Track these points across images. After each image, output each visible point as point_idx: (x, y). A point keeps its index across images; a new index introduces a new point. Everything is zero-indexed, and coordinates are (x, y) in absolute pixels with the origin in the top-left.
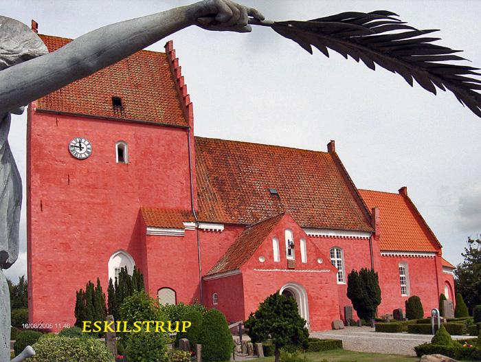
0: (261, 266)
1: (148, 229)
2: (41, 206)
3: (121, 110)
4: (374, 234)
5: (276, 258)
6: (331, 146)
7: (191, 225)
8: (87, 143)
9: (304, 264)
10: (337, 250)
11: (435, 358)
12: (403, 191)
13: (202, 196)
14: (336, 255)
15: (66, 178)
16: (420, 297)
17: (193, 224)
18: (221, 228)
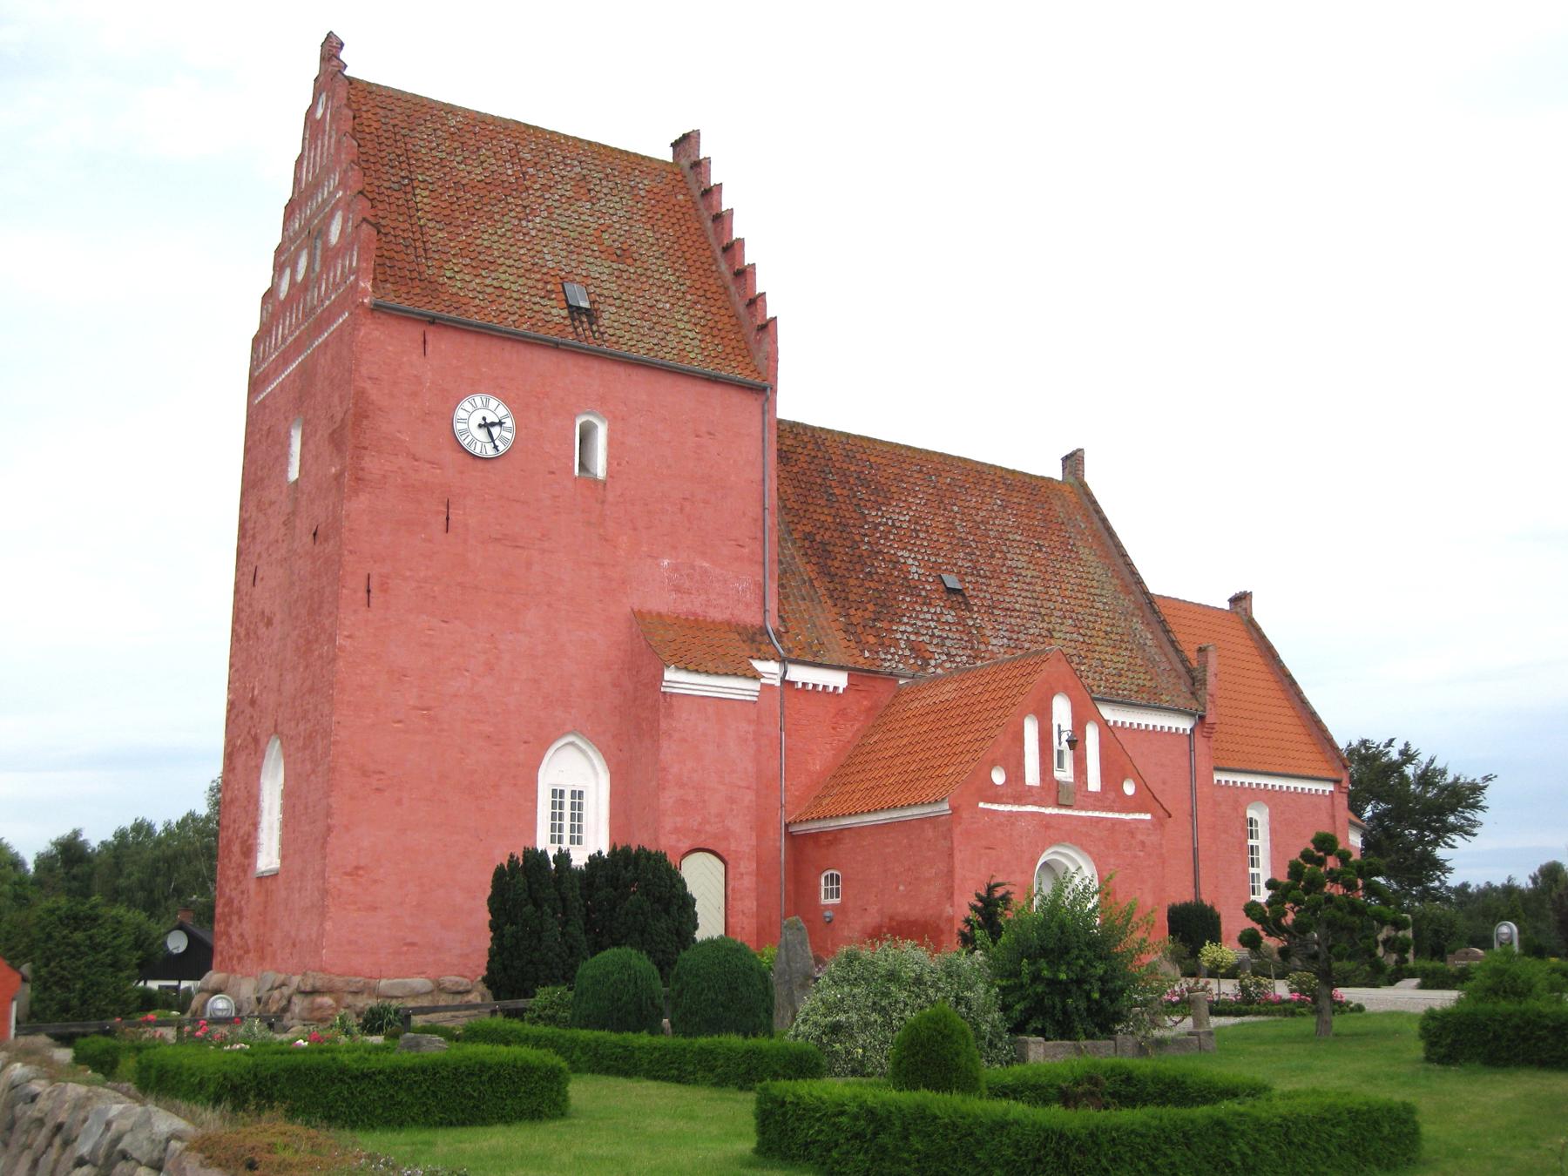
0: (996, 795)
1: (670, 675)
2: (369, 591)
3: (591, 324)
4: (1202, 718)
5: (1032, 776)
6: (1073, 462)
7: (769, 669)
9: (1031, 787)
12: (1241, 600)
15: (438, 513)
16: (1169, 902)
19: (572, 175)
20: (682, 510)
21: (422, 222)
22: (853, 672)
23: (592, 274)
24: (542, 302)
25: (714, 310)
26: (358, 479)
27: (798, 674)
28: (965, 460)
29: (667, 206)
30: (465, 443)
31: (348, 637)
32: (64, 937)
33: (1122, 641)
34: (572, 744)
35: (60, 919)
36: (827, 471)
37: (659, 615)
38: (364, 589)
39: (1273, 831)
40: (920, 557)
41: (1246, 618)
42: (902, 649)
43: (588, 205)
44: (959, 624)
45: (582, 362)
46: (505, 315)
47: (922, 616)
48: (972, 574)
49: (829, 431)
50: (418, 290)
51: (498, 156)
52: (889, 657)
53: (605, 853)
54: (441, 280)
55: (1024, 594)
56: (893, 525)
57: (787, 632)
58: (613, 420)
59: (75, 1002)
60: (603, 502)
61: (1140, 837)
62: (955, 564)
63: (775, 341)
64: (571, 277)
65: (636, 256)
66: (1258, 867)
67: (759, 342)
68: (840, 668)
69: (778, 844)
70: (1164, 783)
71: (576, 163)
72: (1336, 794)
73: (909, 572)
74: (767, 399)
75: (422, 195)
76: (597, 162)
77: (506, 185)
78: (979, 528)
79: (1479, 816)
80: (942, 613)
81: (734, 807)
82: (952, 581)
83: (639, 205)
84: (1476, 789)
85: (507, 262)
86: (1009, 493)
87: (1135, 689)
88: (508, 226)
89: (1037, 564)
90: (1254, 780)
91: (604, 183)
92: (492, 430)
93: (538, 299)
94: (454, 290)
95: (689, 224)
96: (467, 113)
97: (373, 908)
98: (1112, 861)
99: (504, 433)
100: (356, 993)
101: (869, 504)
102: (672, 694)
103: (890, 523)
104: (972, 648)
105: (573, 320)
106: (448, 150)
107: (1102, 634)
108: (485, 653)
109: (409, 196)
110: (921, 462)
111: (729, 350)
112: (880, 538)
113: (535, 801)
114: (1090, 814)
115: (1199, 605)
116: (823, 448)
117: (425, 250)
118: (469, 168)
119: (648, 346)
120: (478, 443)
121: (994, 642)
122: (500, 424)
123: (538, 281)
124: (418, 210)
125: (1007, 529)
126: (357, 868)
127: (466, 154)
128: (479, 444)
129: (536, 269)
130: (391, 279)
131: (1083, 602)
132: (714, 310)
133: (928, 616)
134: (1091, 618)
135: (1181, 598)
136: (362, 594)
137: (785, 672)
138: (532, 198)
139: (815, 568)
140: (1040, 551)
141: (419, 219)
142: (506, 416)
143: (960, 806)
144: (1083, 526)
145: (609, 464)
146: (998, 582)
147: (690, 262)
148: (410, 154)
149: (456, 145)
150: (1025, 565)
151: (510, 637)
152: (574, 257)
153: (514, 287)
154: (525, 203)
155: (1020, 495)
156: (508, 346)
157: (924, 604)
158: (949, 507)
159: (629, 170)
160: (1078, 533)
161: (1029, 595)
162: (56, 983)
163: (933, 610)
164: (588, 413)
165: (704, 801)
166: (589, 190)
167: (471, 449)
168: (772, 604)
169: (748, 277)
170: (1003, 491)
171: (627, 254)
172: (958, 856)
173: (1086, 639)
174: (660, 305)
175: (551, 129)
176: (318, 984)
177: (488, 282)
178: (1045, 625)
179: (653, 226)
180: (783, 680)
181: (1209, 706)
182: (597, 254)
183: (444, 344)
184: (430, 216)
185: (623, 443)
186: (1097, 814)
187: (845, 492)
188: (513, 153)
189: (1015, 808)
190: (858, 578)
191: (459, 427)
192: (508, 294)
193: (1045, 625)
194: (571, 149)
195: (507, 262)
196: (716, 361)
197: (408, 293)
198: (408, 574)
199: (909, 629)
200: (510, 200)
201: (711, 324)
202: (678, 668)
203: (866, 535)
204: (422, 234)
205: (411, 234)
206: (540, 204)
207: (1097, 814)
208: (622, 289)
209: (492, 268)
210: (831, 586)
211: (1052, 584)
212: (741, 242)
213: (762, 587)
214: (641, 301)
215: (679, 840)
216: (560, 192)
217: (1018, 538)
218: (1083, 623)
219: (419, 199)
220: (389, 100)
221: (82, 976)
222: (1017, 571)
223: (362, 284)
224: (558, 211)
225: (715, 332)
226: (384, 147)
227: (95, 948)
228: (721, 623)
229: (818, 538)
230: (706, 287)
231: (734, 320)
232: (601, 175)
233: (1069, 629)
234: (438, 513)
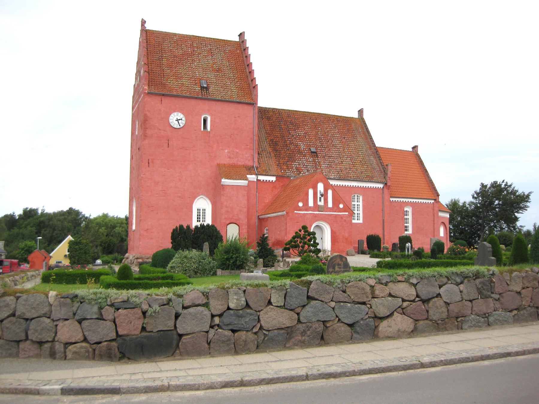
0: (300, 209)
1: (223, 180)
2: (149, 163)
3: (206, 91)
4: (386, 184)
5: (311, 203)
6: (361, 112)
7: (252, 177)
9: (310, 207)
10: (357, 196)
12: (415, 148)
13: (261, 154)
14: (356, 200)
15: (166, 143)
19: (207, 49)
20: (231, 137)
21: (164, 68)
22: (277, 177)
23: (209, 77)
25: (243, 83)
26: (145, 136)
27: (261, 178)
28: (325, 114)
29: (234, 54)
30: (172, 125)
31: (144, 174)
32: (74, 247)
33: (365, 163)
34: (202, 197)
35: (73, 243)
36: (281, 121)
37: (224, 164)
38: (148, 163)
39: (413, 214)
40: (305, 143)
41: (415, 153)
42: (294, 169)
43: (211, 57)
44: (313, 161)
45: (203, 101)
46: (183, 91)
47: (302, 160)
48: (321, 147)
49: (284, 110)
50: (160, 87)
51: (187, 46)
52: (289, 172)
53: (210, 224)
54: (167, 83)
55: (336, 152)
56: (299, 135)
57: (260, 167)
58: (211, 115)
59: (76, 261)
60: (209, 137)
61: (344, 219)
62: (316, 145)
63: (257, 91)
64: (203, 78)
65: (222, 70)
66: (409, 224)
67: (253, 91)
68: (273, 176)
69: (255, 221)
70: (374, 202)
71: (209, 45)
72: (435, 203)
73: (301, 148)
74: (255, 106)
75: (164, 61)
76: (215, 44)
77: (188, 54)
78: (326, 134)
79: (528, 204)
80: (308, 159)
81: (241, 212)
82: (313, 149)
83: (226, 55)
84: (528, 196)
85: (186, 76)
86: (338, 123)
87: (365, 176)
88: (187, 66)
89: (342, 143)
90: (407, 200)
91: (216, 50)
92: (179, 121)
93: (193, 86)
94: (170, 86)
95: (240, 59)
96: (179, 35)
97: (152, 239)
98: (335, 225)
99: (182, 122)
100: (147, 259)
101: (292, 130)
102: (224, 185)
103: (298, 134)
104: (316, 168)
105: (202, 90)
106: (173, 47)
107: (359, 162)
108: (179, 176)
109: (161, 61)
110: (311, 116)
111: (245, 94)
112: (293, 139)
113: (192, 212)
114: (329, 213)
115: (401, 150)
116: (281, 115)
117: (164, 76)
118: (178, 51)
119: (222, 95)
120: (175, 125)
121: (323, 166)
122: (181, 119)
123: (193, 80)
124: (163, 65)
125: (334, 134)
126: (147, 229)
127: (178, 47)
128: (176, 125)
129: (193, 77)
130: (154, 85)
131: (355, 153)
132: (243, 83)
133: (304, 160)
134: (356, 157)
135: (394, 148)
136: (147, 164)
137: (257, 178)
138: (195, 57)
139: (272, 149)
140: (344, 139)
141: (163, 67)
142: (183, 117)
143: (289, 212)
144: (360, 130)
145: (211, 127)
146: (328, 149)
147: (238, 70)
148: (163, 49)
149: (176, 45)
150: (338, 143)
151: (185, 172)
152: (205, 72)
153: (186, 83)
154: (193, 59)
155: (341, 123)
156: (183, 99)
157: (303, 156)
158: (317, 128)
159: (224, 45)
160: (358, 133)
161: (338, 152)
162: (73, 257)
163: (306, 158)
164: (206, 114)
165: (233, 211)
166: (212, 53)
167: (174, 126)
168: (256, 160)
169: (252, 73)
170: (336, 122)
171: (220, 70)
172: (288, 225)
173: (353, 163)
174: (227, 83)
175: (203, 36)
176: (138, 256)
177: (179, 82)
178: (341, 160)
179: (229, 61)
180: (257, 180)
181: (388, 181)
182: (211, 71)
183: (166, 100)
184: (166, 66)
185: (215, 121)
186: (331, 213)
187: (285, 127)
188: (191, 45)
189: (306, 212)
190: (284, 151)
191: (170, 121)
192: (185, 85)
193: (341, 160)
194: (208, 41)
196: (241, 97)
197: (158, 88)
198: (158, 158)
199: (297, 164)
200: (189, 58)
201: (241, 87)
202: (225, 179)
203: (289, 138)
204: (163, 71)
205: (160, 72)
206: (197, 59)
207: (331, 213)
208: (217, 80)
209: (181, 78)
210: (276, 153)
211: (346, 148)
212: (251, 63)
213: (253, 156)
214: (222, 83)
215: (226, 221)
216: (203, 54)
217: (338, 136)
218: (353, 159)
219: (164, 61)
220: (158, 35)
221: (78, 256)
222: (335, 145)
223: (145, 88)
224: (202, 60)
225: (242, 89)
226: (155, 48)
227: (80, 249)
228: (242, 165)
229: (274, 141)
230: (242, 77)
231: (248, 85)
232: (216, 48)
233: (348, 161)
234: (166, 143)
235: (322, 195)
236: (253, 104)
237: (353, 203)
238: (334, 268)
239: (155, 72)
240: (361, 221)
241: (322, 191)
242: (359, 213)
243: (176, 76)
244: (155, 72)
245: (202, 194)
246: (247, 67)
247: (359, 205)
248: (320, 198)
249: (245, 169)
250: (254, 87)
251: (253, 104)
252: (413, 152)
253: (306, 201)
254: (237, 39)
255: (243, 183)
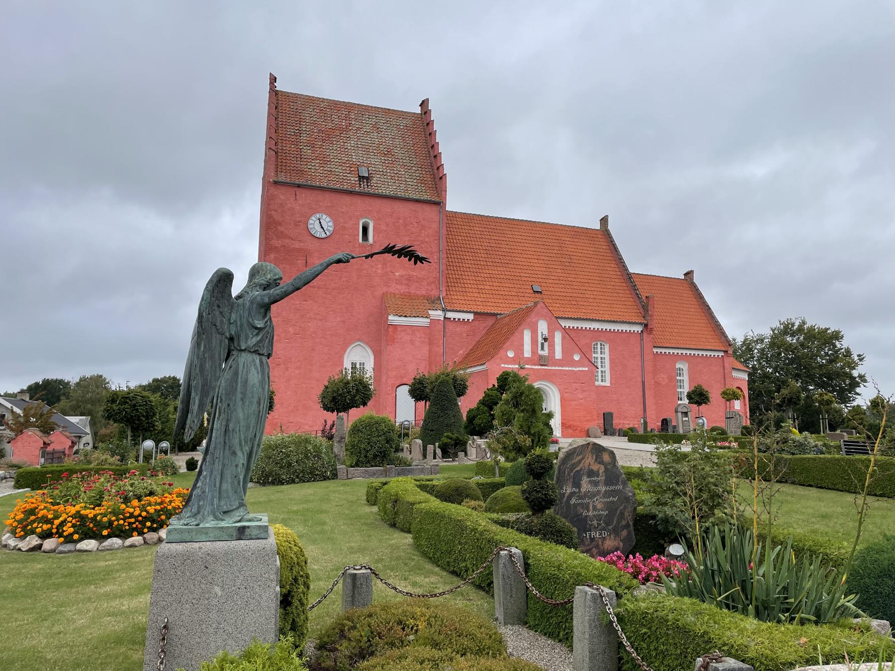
1: (391, 317)
3: (367, 183)
5: (527, 354)
6: (604, 221)
7: (437, 314)
8: (328, 219)
10: (601, 345)
11: (803, 595)
12: (689, 274)
14: (599, 350)
17: (440, 313)
18: (471, 317)
22: (475, 313)
24: (348, 175)
27: (450, 315)
34: (359, 345)
50: (295, 174)
58: (377, 221)
75: (304, 138)
145: (374, 237)
164: (366, 218)
180: (445, 318)
183: (303, 194)
184: (305, 144)
191: (310, 226)
195: (336, 161)
214: (392, 172)
219: (302, 138)
235: (545, 339)
236: (437, 204)
237: (594, 355)
238: (577, 485)
239: (288, 152)
240: (608, 384)
241: (546, 332)
242: (605, 371)
243: (321, 159)
244: (288, 152)
245: (359, 340)
246: (430, 149)
247: (604, 358)
248: (542, 344)
249: (426, 301)
250: (441, 178)
251: (437, 204)
252: (685, 280)
253: (520, 349)
254: (418, 110)
255: (423, 322)
